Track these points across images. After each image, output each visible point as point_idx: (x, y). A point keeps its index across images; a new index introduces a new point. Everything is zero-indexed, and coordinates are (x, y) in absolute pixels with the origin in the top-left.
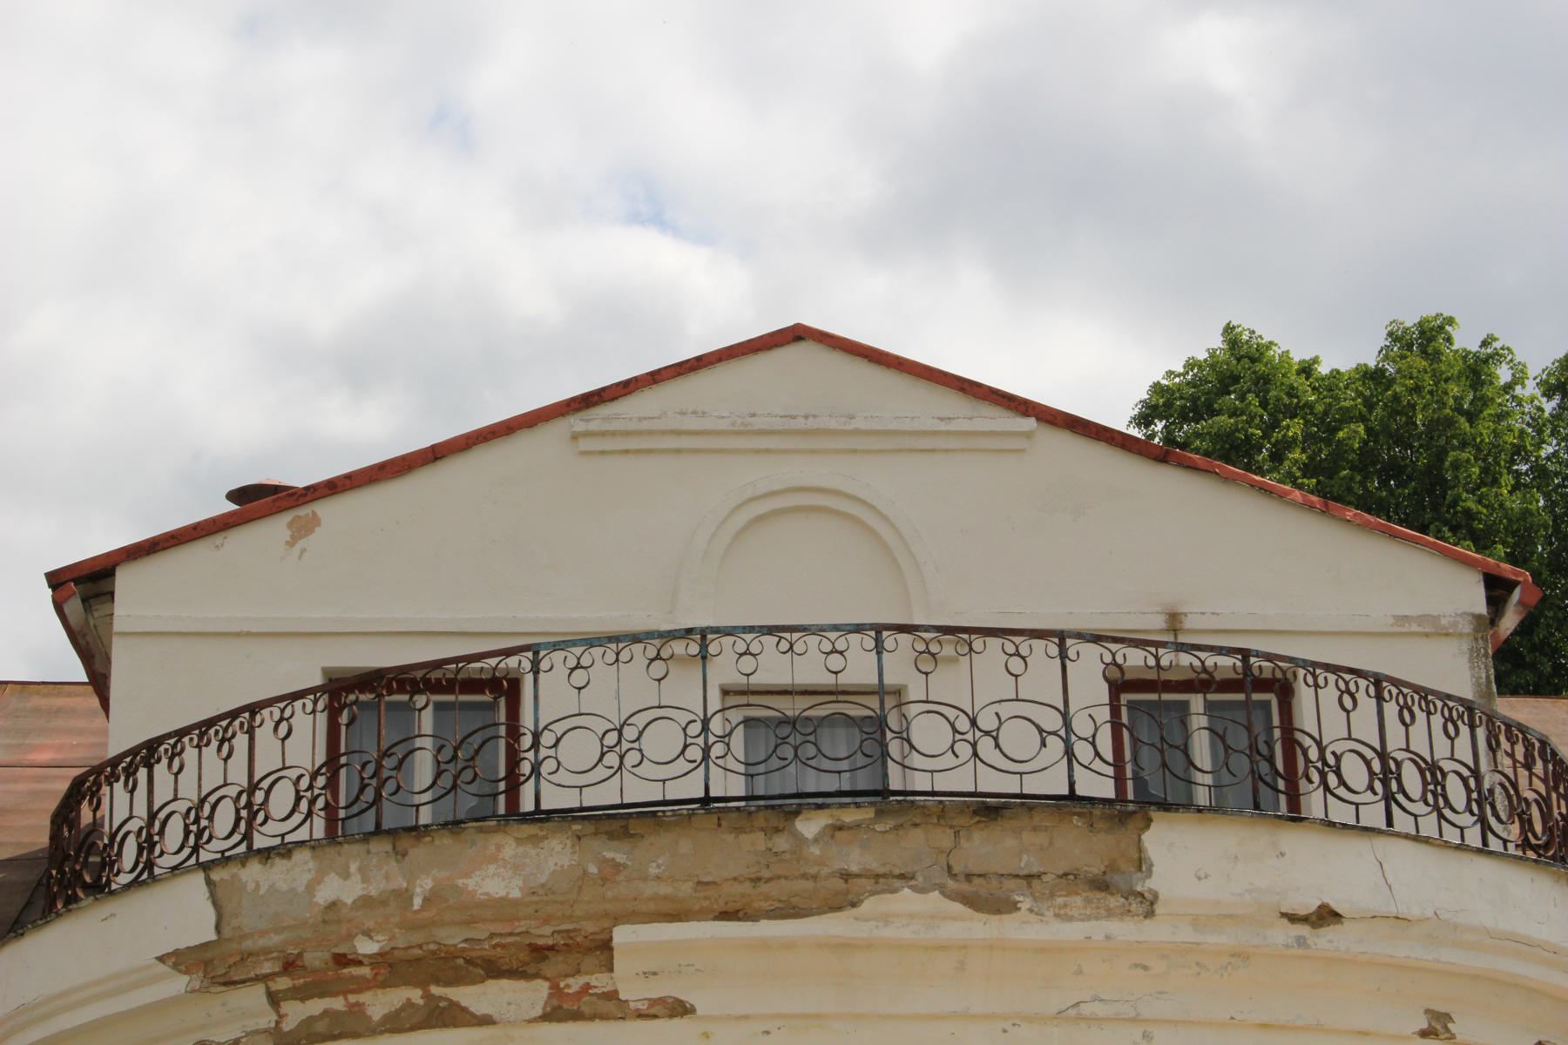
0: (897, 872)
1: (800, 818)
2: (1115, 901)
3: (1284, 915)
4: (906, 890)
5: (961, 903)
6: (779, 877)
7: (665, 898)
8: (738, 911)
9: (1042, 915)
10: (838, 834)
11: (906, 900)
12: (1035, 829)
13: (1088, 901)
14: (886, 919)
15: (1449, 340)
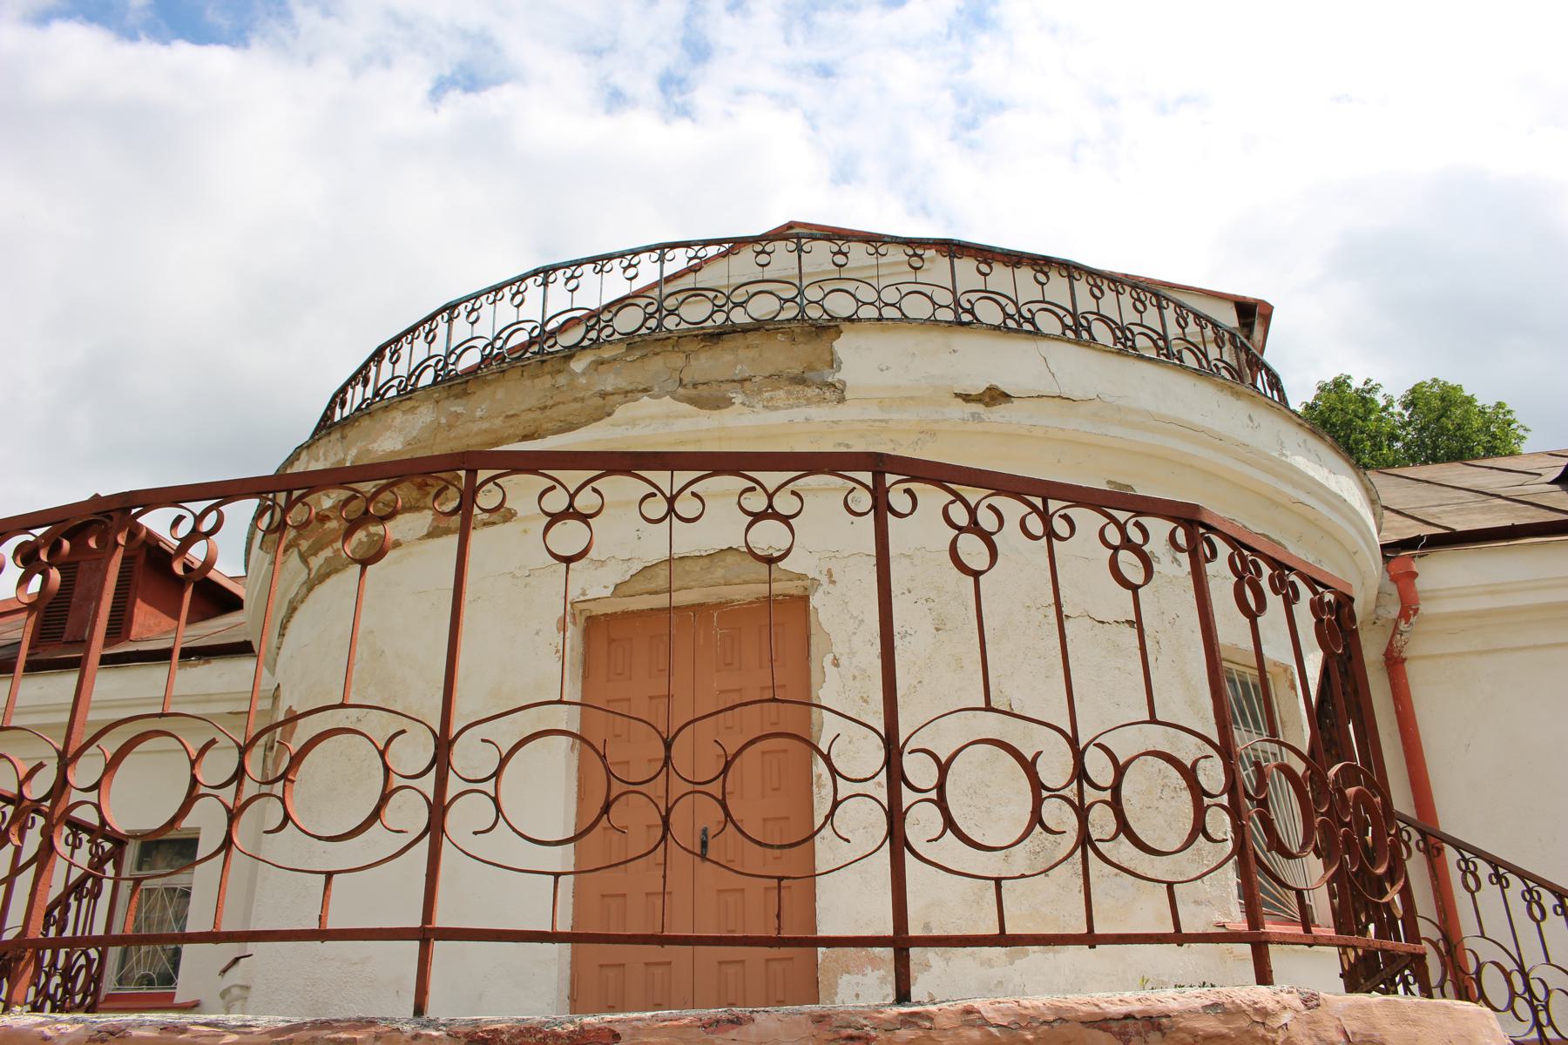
0: (641, 387)
1: (574, 360)
2: (812, 392)
3: (957, 395)
4: (645, 397)
5: (688, 403)
6: (559, 403)
7: (485, 431)
8: (534, 433)
9: (753, 407)
10: (600, 367)
11: (645, 404)
12: (748, 347)
13: (789, 393)
14: (633, 422)
15: (1349, 386)
